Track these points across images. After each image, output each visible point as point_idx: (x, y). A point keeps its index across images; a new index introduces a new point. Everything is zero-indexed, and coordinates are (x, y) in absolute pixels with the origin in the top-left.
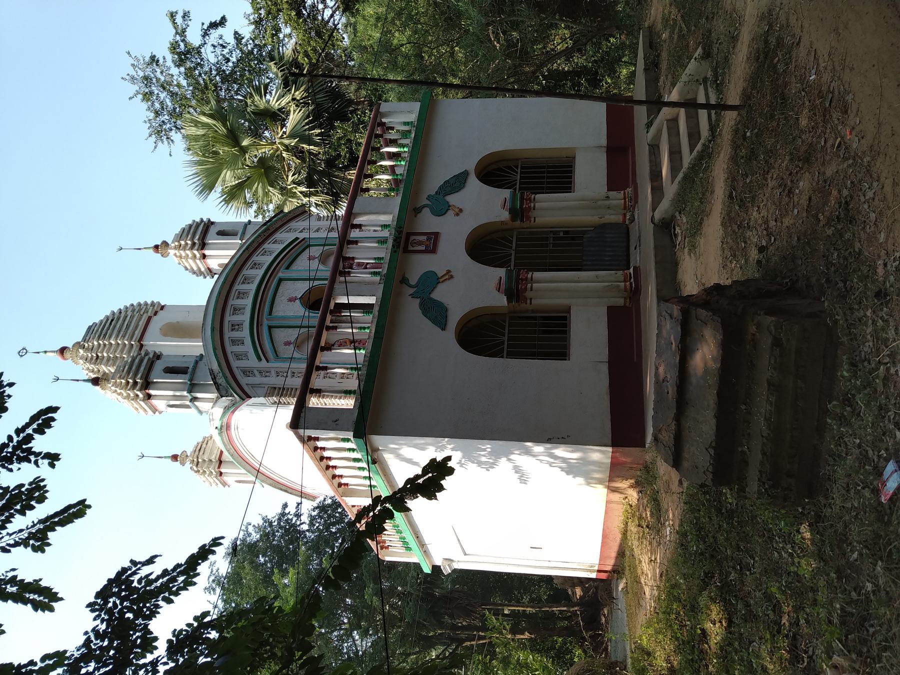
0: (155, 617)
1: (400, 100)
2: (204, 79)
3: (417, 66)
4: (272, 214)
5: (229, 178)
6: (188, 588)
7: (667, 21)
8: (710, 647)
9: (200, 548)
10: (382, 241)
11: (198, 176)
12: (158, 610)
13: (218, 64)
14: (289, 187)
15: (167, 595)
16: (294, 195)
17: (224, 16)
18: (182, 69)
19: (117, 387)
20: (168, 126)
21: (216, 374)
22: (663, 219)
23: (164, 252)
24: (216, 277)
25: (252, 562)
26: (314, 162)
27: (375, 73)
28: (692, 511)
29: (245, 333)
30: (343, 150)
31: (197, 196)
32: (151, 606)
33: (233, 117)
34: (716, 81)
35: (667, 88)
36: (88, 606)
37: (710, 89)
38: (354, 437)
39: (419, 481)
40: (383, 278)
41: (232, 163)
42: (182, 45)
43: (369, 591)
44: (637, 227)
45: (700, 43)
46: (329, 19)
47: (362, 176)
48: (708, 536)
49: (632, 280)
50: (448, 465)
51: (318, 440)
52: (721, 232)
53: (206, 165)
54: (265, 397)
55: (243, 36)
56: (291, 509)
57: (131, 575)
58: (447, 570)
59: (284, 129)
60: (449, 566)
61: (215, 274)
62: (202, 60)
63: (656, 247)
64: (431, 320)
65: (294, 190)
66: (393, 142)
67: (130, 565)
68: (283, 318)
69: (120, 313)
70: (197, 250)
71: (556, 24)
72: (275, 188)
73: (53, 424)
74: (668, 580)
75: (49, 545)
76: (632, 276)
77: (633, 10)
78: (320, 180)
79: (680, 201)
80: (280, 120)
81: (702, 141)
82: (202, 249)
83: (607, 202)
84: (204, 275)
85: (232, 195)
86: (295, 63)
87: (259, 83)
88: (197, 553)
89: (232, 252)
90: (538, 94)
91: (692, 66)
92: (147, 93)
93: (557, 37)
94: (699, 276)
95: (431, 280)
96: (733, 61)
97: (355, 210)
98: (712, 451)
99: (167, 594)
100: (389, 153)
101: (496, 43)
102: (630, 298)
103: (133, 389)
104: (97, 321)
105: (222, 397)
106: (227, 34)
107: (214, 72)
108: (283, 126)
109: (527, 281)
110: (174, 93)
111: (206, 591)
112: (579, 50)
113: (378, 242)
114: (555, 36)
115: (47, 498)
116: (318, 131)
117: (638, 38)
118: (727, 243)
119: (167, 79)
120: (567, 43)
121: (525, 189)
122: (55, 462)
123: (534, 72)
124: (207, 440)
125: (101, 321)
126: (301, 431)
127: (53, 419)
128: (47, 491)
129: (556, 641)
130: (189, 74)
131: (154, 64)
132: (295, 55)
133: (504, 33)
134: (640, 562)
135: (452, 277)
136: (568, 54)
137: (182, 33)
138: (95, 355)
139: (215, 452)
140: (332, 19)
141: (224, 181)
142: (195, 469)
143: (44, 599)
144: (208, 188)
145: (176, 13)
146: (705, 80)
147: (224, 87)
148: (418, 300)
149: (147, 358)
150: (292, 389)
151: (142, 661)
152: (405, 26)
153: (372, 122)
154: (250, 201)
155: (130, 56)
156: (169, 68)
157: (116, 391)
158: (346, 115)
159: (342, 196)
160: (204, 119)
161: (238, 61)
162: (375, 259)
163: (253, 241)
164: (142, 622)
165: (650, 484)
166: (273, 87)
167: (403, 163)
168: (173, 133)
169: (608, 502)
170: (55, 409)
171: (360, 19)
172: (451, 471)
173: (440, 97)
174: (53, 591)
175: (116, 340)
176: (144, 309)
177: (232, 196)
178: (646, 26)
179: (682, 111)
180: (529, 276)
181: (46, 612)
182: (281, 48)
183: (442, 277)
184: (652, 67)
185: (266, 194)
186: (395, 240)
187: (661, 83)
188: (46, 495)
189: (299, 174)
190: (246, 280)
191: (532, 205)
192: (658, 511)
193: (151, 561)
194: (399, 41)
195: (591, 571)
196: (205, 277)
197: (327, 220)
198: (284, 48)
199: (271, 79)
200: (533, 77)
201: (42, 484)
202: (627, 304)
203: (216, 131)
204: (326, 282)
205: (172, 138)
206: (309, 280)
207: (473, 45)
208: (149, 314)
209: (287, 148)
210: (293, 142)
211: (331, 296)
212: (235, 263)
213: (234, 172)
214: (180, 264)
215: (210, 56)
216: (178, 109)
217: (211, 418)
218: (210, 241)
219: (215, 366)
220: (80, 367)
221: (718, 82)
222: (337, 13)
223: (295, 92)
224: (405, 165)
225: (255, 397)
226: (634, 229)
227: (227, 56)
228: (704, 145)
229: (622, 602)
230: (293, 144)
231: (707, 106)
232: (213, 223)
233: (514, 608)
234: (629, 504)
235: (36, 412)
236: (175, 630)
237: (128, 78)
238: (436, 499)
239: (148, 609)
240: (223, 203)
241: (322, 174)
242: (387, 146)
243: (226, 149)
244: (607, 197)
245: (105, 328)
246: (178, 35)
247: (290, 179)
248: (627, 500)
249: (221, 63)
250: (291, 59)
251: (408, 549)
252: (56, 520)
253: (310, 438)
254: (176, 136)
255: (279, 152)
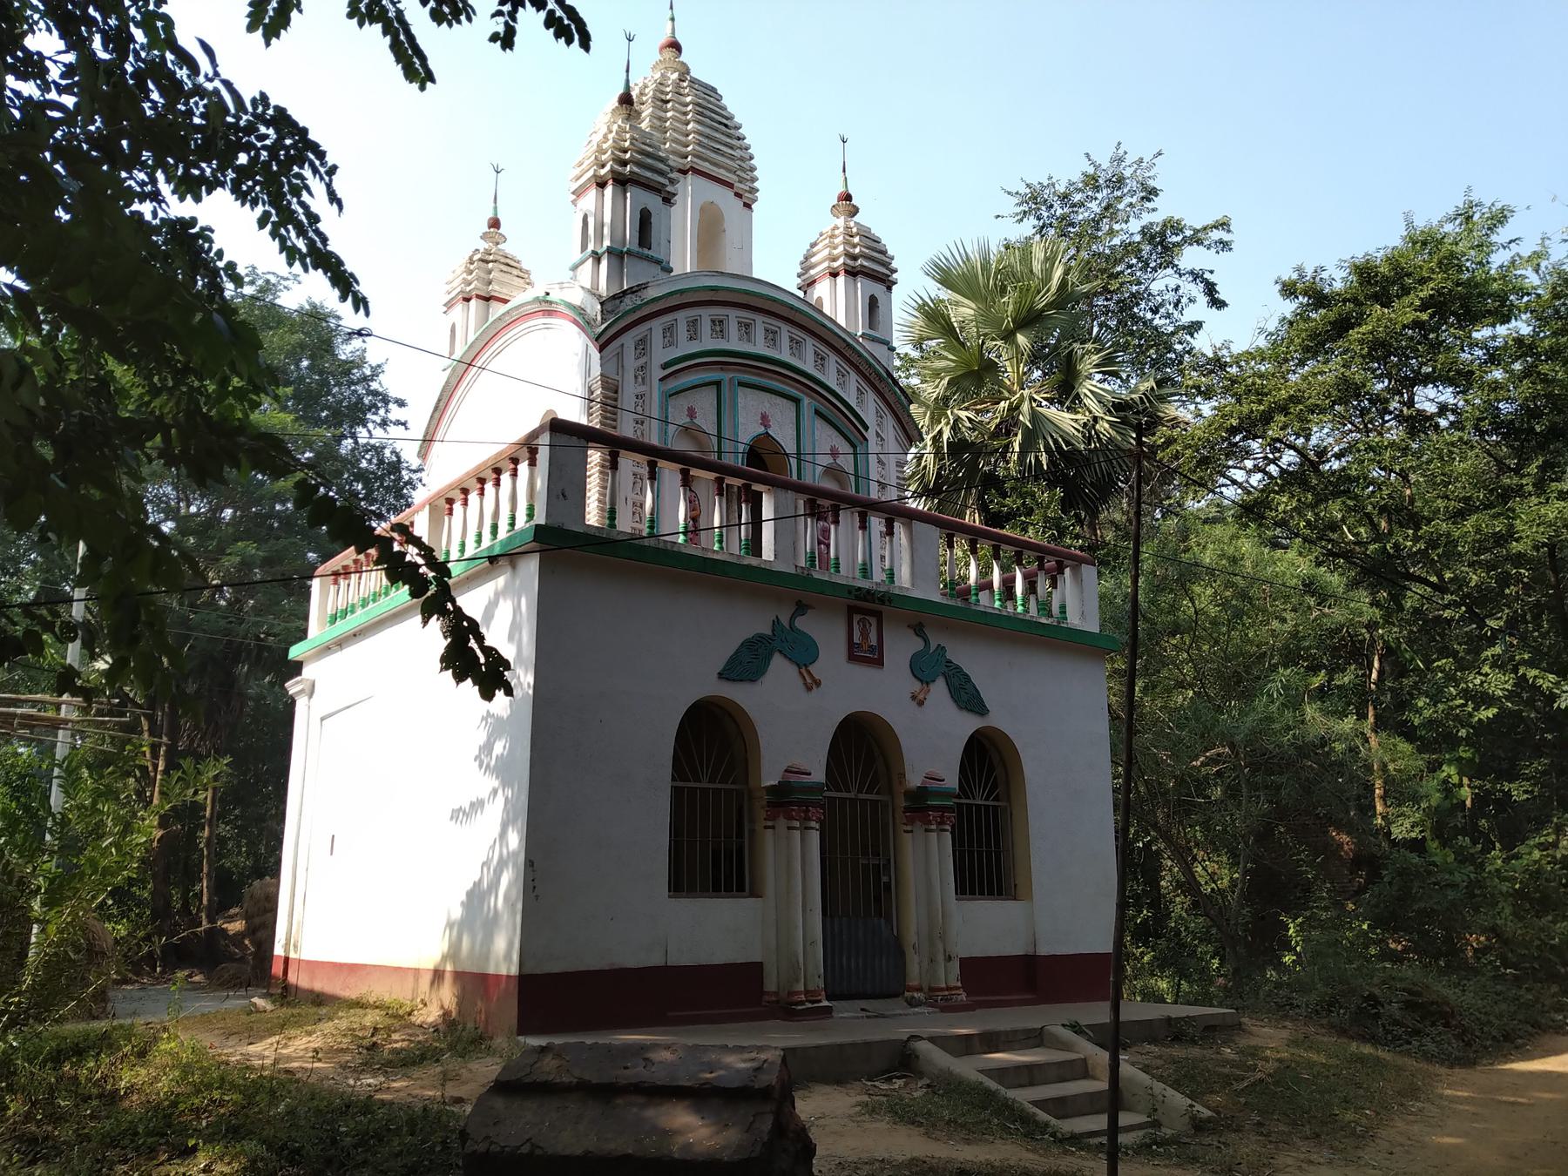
0: (237, 199)
1: (1102, 597)
2: (1122, 272)
3: (1159, 627)
4: (903, 382)
5: (963, 311)
6: (284, 254)
7: (1253, 1055)
8: (161, 1164)
9: (352, 275)
10: (866, 571)
11: (964, 262)
12: (248, 204)
13: (1148, 296)
14: (949, 412)
15: (272, 219)
16: (935, 420)
17: (1227, 305)
18: (1138, 238)
19: (617, 133)
20: (1045, 214)
21: (639, 293)
22: (917, 1057)
23: (841, 209)
24: (801, 294)
25: (302, 346)
26: (991, 454)
27: (1147, 551)
28: (412, 1123)
29: (708, 342)
30: (1014, 502)
31: (932, 259)
32: (256, 194)
33: (1063, 320)
34: (1156, 1143)
35: (1139, 1058)
36: (263, 95)
37: (1141, 1133)
38: (537, 525)
39: (472, 641)
40: (806, 572)
41: (987, 317)
42: (1175, 239)
43: (251, 548)
44: (901, 1012)
45: (1218, 1113)
46: (1228, 478)
47: (974, 536)
48: (367, 1151)
49: (810, 1005)
50: (497, 691)
51: (530, 465)
52: (901, 1159)
53: (983, 275)
54: (601, 375)
55: (1195, 334)
56: (395, 413)
57: (312, 165)
58: (292, 687)
59: (1044, 403)
60: (302, 691)
61: (805, 293)
62: (1154, 269)
63: (868, 1044)
64: (736, 653)
65: (943, 421)
66: (1031, 587)
67: (330, 164)
68: (734, 406)
69: (739, 139)
70: (844, 264)
71: (1239, 863)
72: (946, 389)
73: (562, 41)
74: (281, 1084)
75: (361, 25)
76: (816, 1005)
77: (1269, 996)
78: (961, 464)
79: (949, 1086)
80: (1061, 396)
81: (1053, 1121)
82: (846, 272)
83: (941, 958)
84: (803, 274)
85: (934, 317)
86: (1155, 421)
87: (1119, 362)
88: (345, 271)
89: (841, 321)
90: (1121, 833)
91: (1179, 1100)
92: (1097, 181)
93: (1216, 867)
94: (822, 1122)
95: (803, 655)
96: (1192, 1171)
97: (917, 525)
98: (525, 1149)
99: (274, 218)
100: (1013, 579)
101: (1202, 759)
102: (778, 1002)
103: (613, 160)
104: (724, 102)
105: (602, 304)
106: (1198, 310)
107: (1135, 288)
108: (1051, 401)
109: (805, 819)
110: (1098, 224)
111: (250, 269)
112: (1195, 905)
113: (864, 564)
114: (1217, 862)
115: (439, 24)
116: (1044, 458)
117: (1220, 1005)
118: (882, 1170)
119: (1120, 213)
120: (1206, 883)
121: (960, 815)
122: (499, 43)
123: (1155, 826)
124: (524, 276)
125: (724, 108)
126: (545, 439)
127: (569, 42)
128: (450, 25)
129: (144, 888)
130: (1130, 248)
131: (1143, 194)
132: (1168, 421)
133: (1219, 774)
134: (309, 1034)
135: (809, 689)
136: (1189, 885)
137: (1196, 239)
138: (668, 97)
139: (504, 291)
140: (1229, 483)
141: (957, 304)
142: (476, 257)
143: (270, 17)
144: (945, 277)
145: (1229, 231)
146: (1156, 1124)
147: (1111, 304)
148: (768, 632)
149: (666, 182)
150: (615, 420)
151: (160, 176)
152: (1225, 605)
153: (1061, 551)
154: (924, 346)
155: (1155, 157)
156: (1138, 217)
157: (611, 132)
158: (1072, 506)
159: (936, 501)
160: (1058, 273)
161: (1156, 328)
162: (837, 558)
163: (860, 355)
164: (228, 178)
165: (451, 1047)
166: (1113, 385)
167: (997, 604)
168: (1032, 221)
169: (417, 972)
170: (585, 44)
171: (1232, 529)
172: (487, 695)
173: (1109, 666)
174: (282, 31)
175: (695, 132)
176: (746, 176)
177: (933, 317)
178: (1243, 1020)
179: (1103, 1085)
180: (813, 824)
181: (248, 20)
182: (1177, 398)
183: (809, 673)
184: (1174, 1031)
185: (937, 374)
186: (868, 591)
187: (1148, 1047)
188: (445, 25)
189: (970, 429)
190: (796, 344)
191: (934, 827)
192: (406, 1062)
193: (333, 198)
194: (1199, 595)
195: (287, 945)
196: (799, 276)
197: (898, 478)
198: (1179, 404)
199: (1127, 380)
200: (1148, 824)
201: (463, 18)
202: (766, 998)
203: (1039, 292)
204: (795, 477)
205: (1025, 220)
206: (799, 453)
207: (1197, 720)
208: (736, 184)
209: (1014, 409)
210: (1024, 419)
211: (773, 486)
212: (824, 326)
213: (972, 321)
214: (821, 235)
215: (1162, 282)
216: (1072, 230)
217: (564, 285)
218: (859, 285)
219: (652, 293)
220: (649, 74)
221: (1154, 1147)
222: (1239, 491)
223: (1108, 421)
224: (994, 608)
225: (601, 359)
226: (896, 1006)
227: (1162, 310)
228: (1047, 1125)
229: (234, 1002)
230: (1021, 418)
231: (1114, 1129)
232: (889, 289)
233: (208, 809)
234: (413, 1011)
235: (581, 15)
236: (212, 231)
237: (1121, 152)
238: (441, 670)
239: (251, 189)
240: (920, 302)
241: (972, 467)
242: (1025, 577)
243: (1011, 307)
244: (950, 957)
245: (713, 115)
246: (1192, 233)
247: (963, 414)
248: (421, 1006)
249: (1150, 301)
250: (1161, 415)
251: (334, 619)
252: (402, 37)
253: (533, 452)
254: (1028, 227)
255: (1007, 394)
